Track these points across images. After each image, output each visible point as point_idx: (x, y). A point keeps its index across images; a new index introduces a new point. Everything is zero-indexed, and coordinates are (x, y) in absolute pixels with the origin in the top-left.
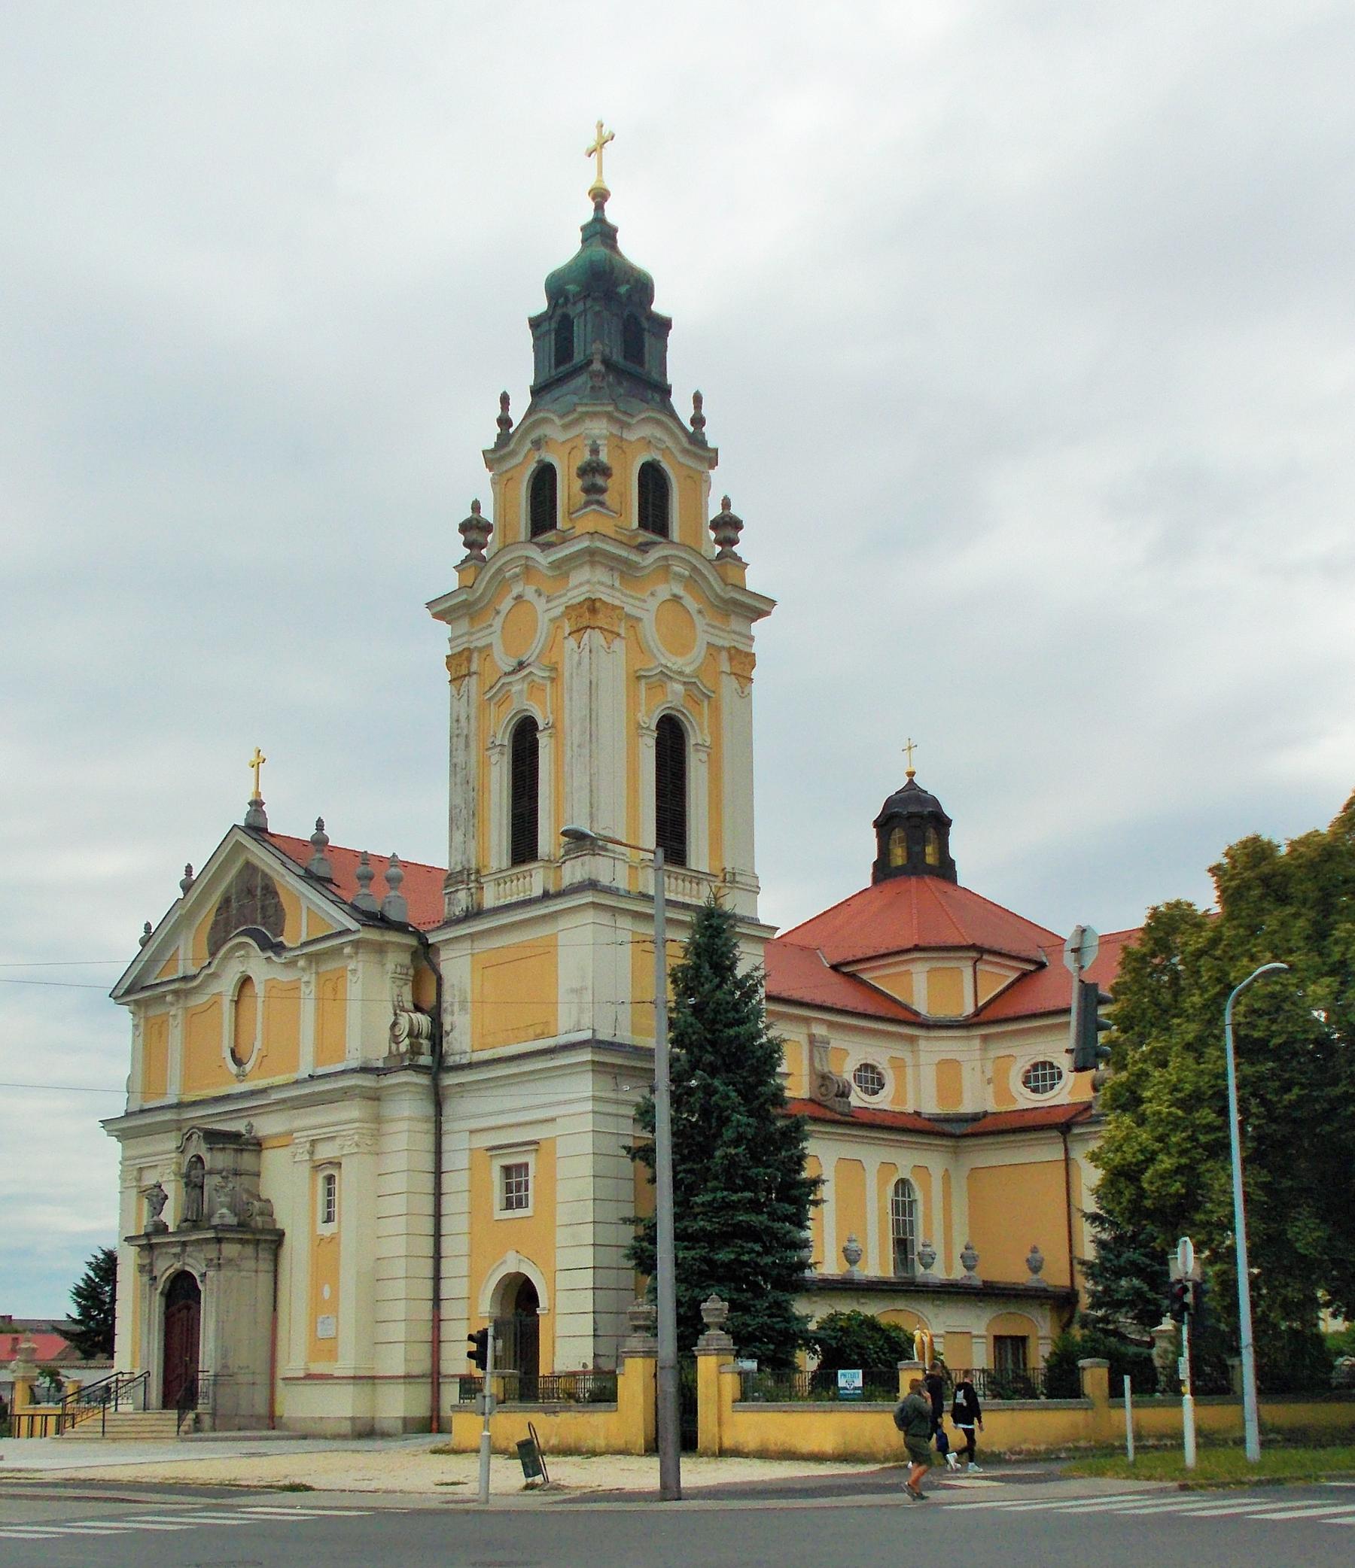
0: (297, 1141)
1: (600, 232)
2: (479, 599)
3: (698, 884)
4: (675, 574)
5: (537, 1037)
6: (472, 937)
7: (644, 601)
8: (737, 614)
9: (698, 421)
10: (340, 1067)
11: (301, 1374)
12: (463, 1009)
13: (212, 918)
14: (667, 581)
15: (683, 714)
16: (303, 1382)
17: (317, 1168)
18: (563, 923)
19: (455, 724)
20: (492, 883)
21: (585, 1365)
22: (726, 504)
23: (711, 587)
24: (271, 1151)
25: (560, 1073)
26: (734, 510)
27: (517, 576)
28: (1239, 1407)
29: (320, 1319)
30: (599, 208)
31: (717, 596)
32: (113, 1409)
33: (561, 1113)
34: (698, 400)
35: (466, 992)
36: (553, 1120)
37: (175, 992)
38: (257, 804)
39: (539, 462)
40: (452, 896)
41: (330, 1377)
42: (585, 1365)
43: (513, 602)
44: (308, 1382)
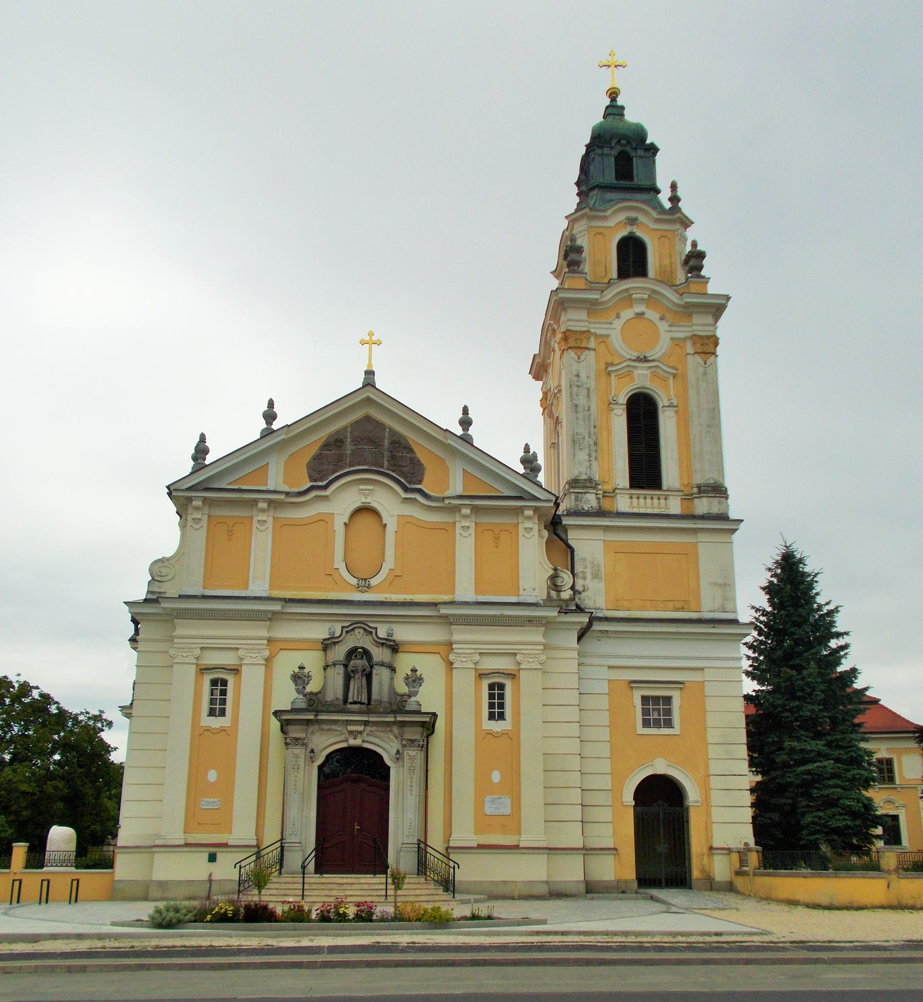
0: (176, 645)
1: (614, 110)
2: (606, 302)
3: (666, 499)
4: (636, 299)
5: (676, 610)
6: (606, 528)
7: (611, 323)
9: (675, 199)
10: (514, 599)
11: (182, 843)
12: (596, 576)
13: (314, 450)
15: (647, 388)
16: (476, 851)
17: (481, 676)
18: (701, 537)
19: (575, 379)
20: (627, 496)
21: (746, 844)
22: (694, 244)
23: (669, 300)
24: (404, 654)
25: (717, 638)
26: (700, 248)
27: (643, 299)
28: (313, 872)
29: (488, 798)
30: (613, 100)
31: (678, 305)
32: (277, 873)
33: (709, 665)
34: (674, 187)
35: (598, 565)
36: (702, 669)
37: (270, 502)
38: (370, 374)
39: (631, 233)
40: (580, 496)
41: (517, 847)
42: (746, 844)
43: (632, 316)
44: (480, 851)
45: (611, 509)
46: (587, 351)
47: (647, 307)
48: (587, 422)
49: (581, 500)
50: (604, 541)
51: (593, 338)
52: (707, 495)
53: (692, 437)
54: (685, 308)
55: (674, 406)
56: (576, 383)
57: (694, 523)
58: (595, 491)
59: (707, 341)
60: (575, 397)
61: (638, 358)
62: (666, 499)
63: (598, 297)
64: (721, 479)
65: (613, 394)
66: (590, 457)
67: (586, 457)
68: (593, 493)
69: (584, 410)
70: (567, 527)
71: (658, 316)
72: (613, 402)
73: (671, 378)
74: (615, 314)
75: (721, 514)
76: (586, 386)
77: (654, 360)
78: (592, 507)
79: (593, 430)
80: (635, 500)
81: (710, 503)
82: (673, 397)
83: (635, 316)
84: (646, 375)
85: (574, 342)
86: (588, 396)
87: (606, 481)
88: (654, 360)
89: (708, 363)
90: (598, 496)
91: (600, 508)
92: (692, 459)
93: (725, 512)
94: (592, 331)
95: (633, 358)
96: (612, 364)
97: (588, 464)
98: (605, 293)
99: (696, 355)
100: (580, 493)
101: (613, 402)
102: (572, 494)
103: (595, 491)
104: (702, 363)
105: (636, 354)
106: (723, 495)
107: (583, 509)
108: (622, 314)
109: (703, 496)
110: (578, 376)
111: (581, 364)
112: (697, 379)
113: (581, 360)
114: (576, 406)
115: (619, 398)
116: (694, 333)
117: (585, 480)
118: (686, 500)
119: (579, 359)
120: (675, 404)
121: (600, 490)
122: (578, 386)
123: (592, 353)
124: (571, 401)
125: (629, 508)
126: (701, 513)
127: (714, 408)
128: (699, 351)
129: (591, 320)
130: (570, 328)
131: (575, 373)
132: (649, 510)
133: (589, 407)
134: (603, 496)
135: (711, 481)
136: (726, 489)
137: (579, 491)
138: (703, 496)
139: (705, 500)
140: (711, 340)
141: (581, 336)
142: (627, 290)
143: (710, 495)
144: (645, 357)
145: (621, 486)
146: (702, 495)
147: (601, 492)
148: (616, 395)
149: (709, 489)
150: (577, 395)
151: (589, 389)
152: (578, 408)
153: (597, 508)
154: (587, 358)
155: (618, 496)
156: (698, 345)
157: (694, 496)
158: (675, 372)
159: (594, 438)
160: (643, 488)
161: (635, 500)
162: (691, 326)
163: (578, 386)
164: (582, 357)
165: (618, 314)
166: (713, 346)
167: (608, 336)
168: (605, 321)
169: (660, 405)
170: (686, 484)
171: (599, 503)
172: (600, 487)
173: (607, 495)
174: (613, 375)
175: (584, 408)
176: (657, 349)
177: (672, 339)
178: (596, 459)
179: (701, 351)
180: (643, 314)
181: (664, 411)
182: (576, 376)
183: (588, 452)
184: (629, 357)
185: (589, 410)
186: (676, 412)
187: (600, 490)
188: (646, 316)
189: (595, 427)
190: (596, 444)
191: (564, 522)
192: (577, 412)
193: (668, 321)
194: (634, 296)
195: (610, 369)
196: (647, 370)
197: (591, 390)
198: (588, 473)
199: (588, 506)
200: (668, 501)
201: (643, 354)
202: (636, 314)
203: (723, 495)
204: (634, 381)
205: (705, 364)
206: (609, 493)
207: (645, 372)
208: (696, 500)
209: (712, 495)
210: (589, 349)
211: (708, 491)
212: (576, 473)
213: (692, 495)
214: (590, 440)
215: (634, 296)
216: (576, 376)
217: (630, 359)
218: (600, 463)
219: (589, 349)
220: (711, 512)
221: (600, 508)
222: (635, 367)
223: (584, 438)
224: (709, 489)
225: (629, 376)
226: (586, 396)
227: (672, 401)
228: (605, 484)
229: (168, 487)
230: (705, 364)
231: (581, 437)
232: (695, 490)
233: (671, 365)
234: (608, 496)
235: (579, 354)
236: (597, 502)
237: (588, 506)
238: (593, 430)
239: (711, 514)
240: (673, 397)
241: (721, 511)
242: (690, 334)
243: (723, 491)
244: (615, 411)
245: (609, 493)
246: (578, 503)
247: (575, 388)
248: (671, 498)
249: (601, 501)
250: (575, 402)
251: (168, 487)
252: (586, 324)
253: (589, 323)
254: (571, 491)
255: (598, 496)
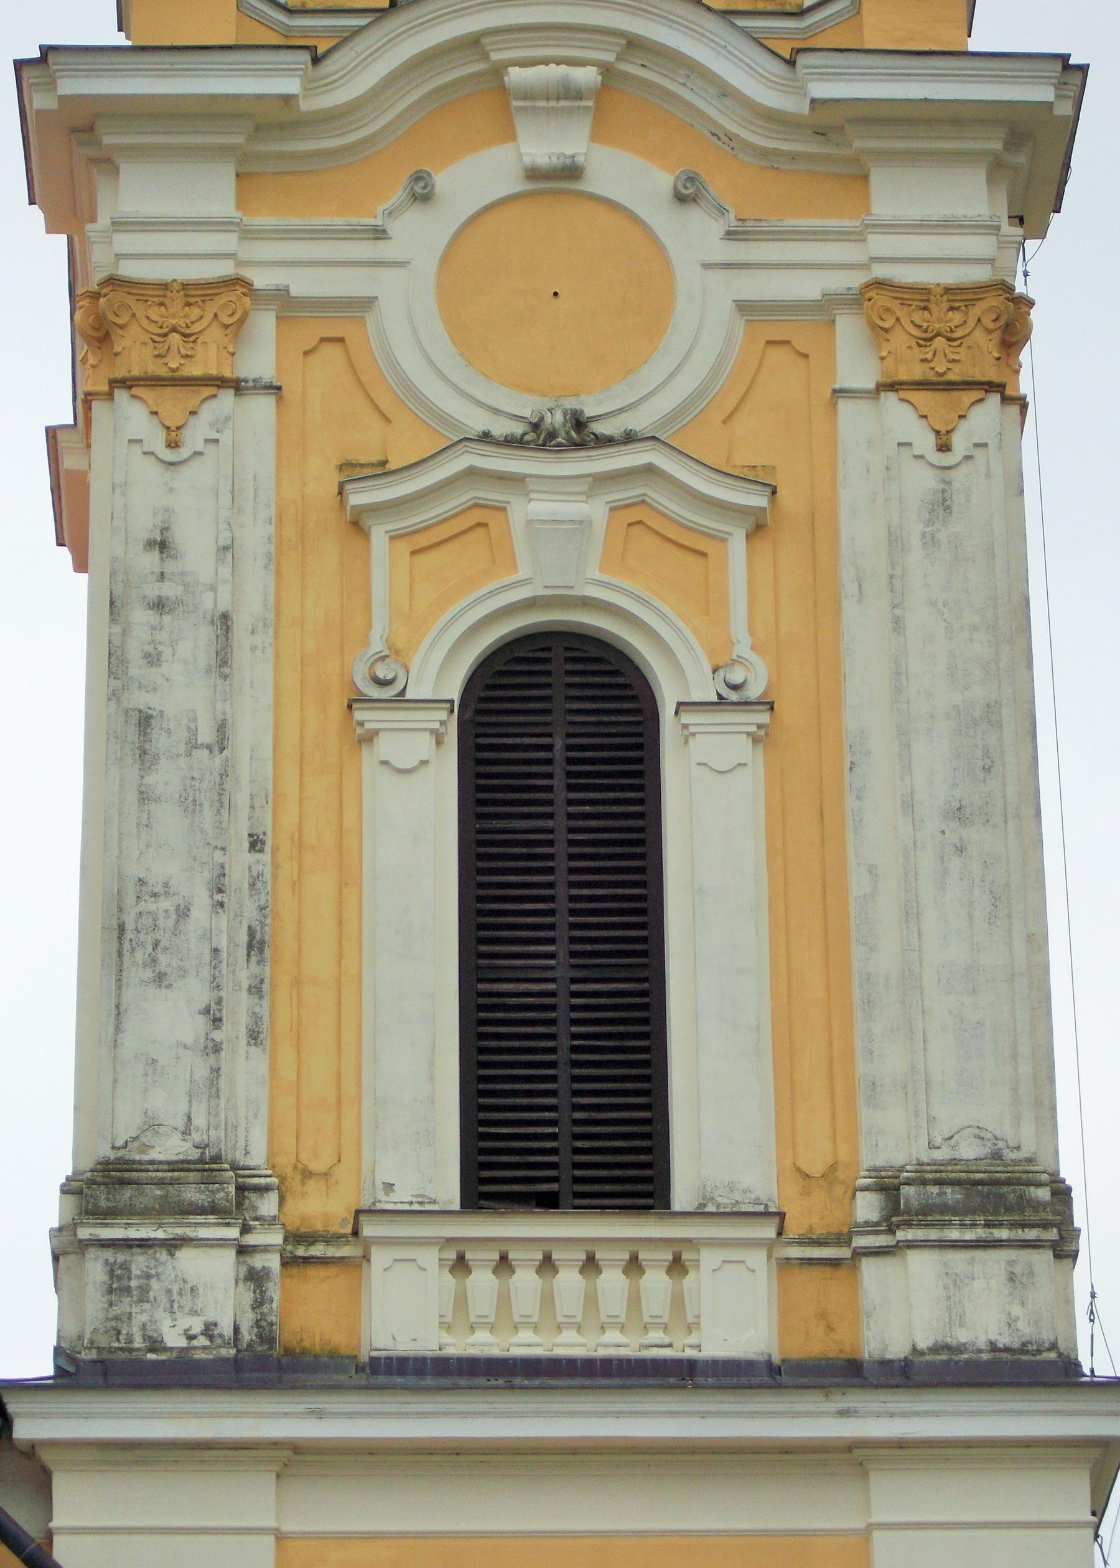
3: (677, 1266)
4: (528, 94)
7: (379, 234)
8: (889, 157)
14: (510, 135)
15: (587, 603)
19: (150, 561)
20: (430, 1257)
23: (726, 91)
27: (569, 93)
40: (139, 1262)
43: (514, 184)
45: (340, 1340)
46: (227, 397)
47: (598, 135)
48: (207, 816)
49: (144, 1290)
50: (281, 1538)
51: (265, 323)
52: (933, 1234)
53: (858, 884)
54: (821, 133)
55: (746, 704)
56: (154, 590)
57: (843, 1413)
58: (233, 1233)
59: (956, 318)
60: (137, 669)
61: (536, 427)
62: (677, 1266)
63: (290, 85)
64: (1028, 1141)
65: (377, 645)
66: (217, 1022)
67: (193, 1027)
68: (221, 1243)
69: (193, 745)
70: (47, 1457)
71: (664, 181)
72: (375, 692)
73: (737, 544)
74: (405, 179)
75: (1023, 1349)
76: (207, 602)
77: (629, 438)
78: (209, 1330)
79: (240, 862)
80: (482, 1280)
81: (955, 1281)
82: (743, 647)
83: (521, 186)
84: (584, 524)
85: (149, 351)
86: (223, 660)
87: (314, 1166)
88: (629, 438)
89: (960, 442)
90: (258, 1261)
91: (265, 1335)
92: (858, 1014)
93: (1047, 1336)
94: (262, 279)
95: (501, 428)
96: (381, 470)
97: (202, 1072)
98: (329, 66)
99: (890, 399)
100: (144, 1244)
101: (375, 692)
102: (92, 1253)
103: (233, 1233)
104: (926, 442)
105: (527, 406)
106: (1031, 1234)
107: (155, 1344)
108: (443, 180)
109: (912, 1245)
110: (162, 545)
111: (188, 472)
112: (895, 541)
113: (185, 452)
114: (145, 721)
115: (415, 665)
116: (880, 271)
117: (174, 1166)
118: (816, 1272)
119: (173, 445)
120: (754, 692)
121: (269, 1222)
122: (159, 605)
123: (262, 407)
124: (114, 696)
125: (446, 1326)
126: (897, 1350)
127: (991, 708)
128: (903, 376)
129: (265, 220)
130: (130, 270)
131: (144, 525)
132: (526, 1336)
133: (222, 727)
134: (288, 1262)
135: (969, 1150)
136: (1062, 1194)
137: (134, 1233)
138: (912, 1245)
139: (921, 1263)
140: (976, 311)
141: (195, 312)
142: (474, 43)
143: (954, 1234)
144: (579, 423)
145: (401, 1198)
146: (900, 1235)
147: (276, 1238)
148: (392, 653)
149: (952, 1195)
150: (153, 659)
151: (225, 619)
152: (154, 733)
153: (247, 1336)
154: (226, 438)
155: (380, 1258)
156: (899, 340)
157: (860, 1241)
158: (758, 500)
159: (250, 912)
160: (548, 1202)
161: (482, 1280)
162: (858, 237)
163: (159, 605)
164: (196, 435)
165: (419, 177)
166: (989, 346)
167: (366, 304)
168: (339, 221)
169: (668, 698)
170: (816, 1168)
171: (258, 1303)
172: (268, 1206)
173: (317, 1250)
174: (379, 536)
175: (194, 732)
176: (652, 374)
177: (744, 307)
178: (254, 1036)
179: (917, 372)
180: (572, 172)
181: (687, 735)
182: (150, 544)
183: (203, 996)
184: (478, 421)
185: (222, 741)
186: (760, 738)
187: (272, 1222)
188: (593, 184)
189: (256, 844)
190: (256, 945)
191: (24, 1430)
192: (145, 756)
193: (722, 211)
194: (516, 75)
195: (358, 498)
196: (589, 495)
197: (242, 622)
198: (199, 1120)
199: (184, 1322)
200: (689, 1280)
201: (570, 404)
202: (533, 174)
203: (1031, 1234)
204: (515, 567)
205: (944, 447)
206: (329, 1239)
207: (573, 508)
208: (869, 1267)
209: (969, 1235)
210: (237, 386)
211: (944, 1209)
212: (126, 1126)
213: (842, 1239)
214: (223, 921)
215: (516, 75)
216: (150, 544)
217: (486, 438)
218: (287, 1056)
219: (237, 386)
220: (962, 1336)
221: (265, 1335)
222: (517, 481)
223: (183, 912)
224: (952, 1195)
225: (479, 533)
226: (205, 659)
227: (737, 677)
228: (311, 1183)
229: (1084, 69)
230: (944, 447)
231: (166, 904)
232: (868, 1207)
233: (742, 458)
234: (324, 1261)
235: (174, 416)
236: (248, 1297)
237: (184, 1322)
238: (240, 862)
239: (959, 1349)
240: (743, 647)
241: (1026, 1330)
242: (855, 280)
243: (1037, 1206)
244: (385, 746)
245: (329, 1239)
246: (124, 1306)
247: (140, 617)
248: (709, 1258)
249: (274, 1291)
250: (141, 700)
251: (1084, 69)
252: (228, 242)
253: (248, 234)
254: (84, 1233)
255: (258, 1261)
